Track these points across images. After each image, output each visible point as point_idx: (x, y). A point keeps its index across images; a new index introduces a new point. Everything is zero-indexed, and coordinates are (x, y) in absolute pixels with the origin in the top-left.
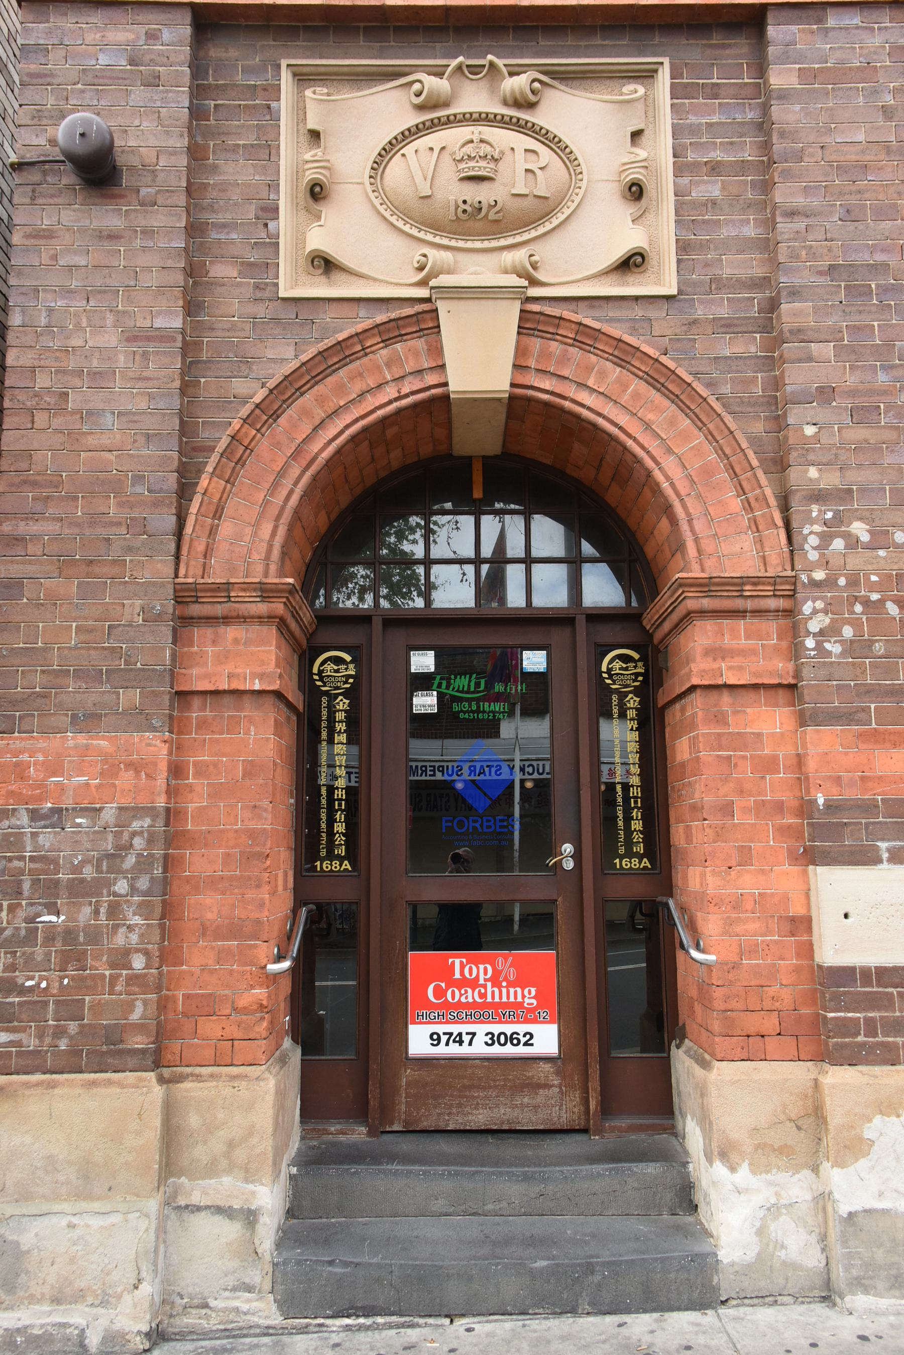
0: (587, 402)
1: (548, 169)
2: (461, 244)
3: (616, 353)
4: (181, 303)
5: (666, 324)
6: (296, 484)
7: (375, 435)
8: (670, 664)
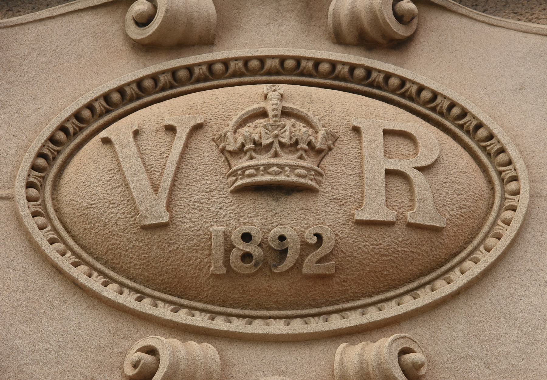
2: (238, 326)
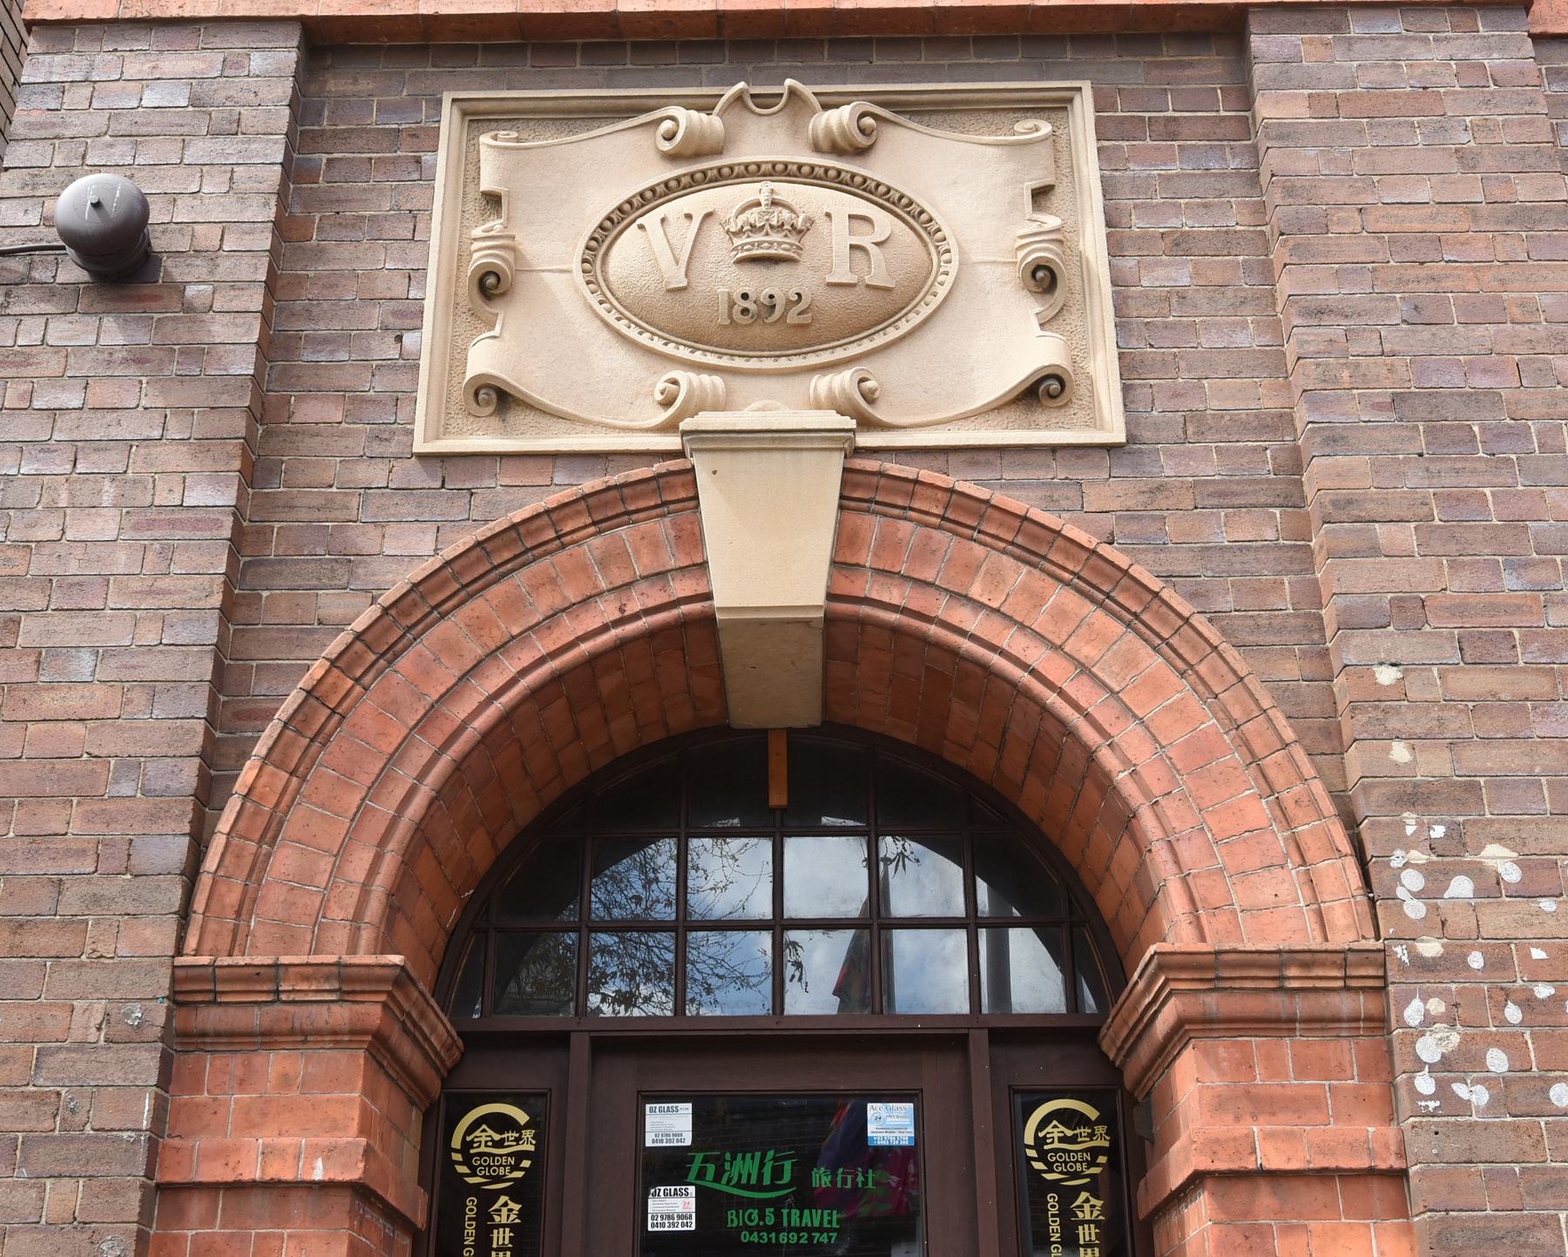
0: (970, 627)
1: (890, 245)
2: (739, 363)
3: (1019, 540)
4: (237, 464)
5: (1108, 492)
6: (421, 777)
7: (575, 688)
8: (1156, 1129)
